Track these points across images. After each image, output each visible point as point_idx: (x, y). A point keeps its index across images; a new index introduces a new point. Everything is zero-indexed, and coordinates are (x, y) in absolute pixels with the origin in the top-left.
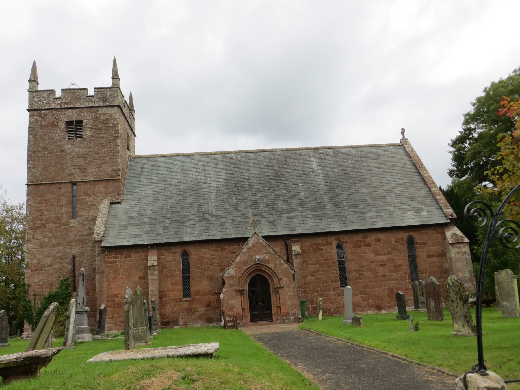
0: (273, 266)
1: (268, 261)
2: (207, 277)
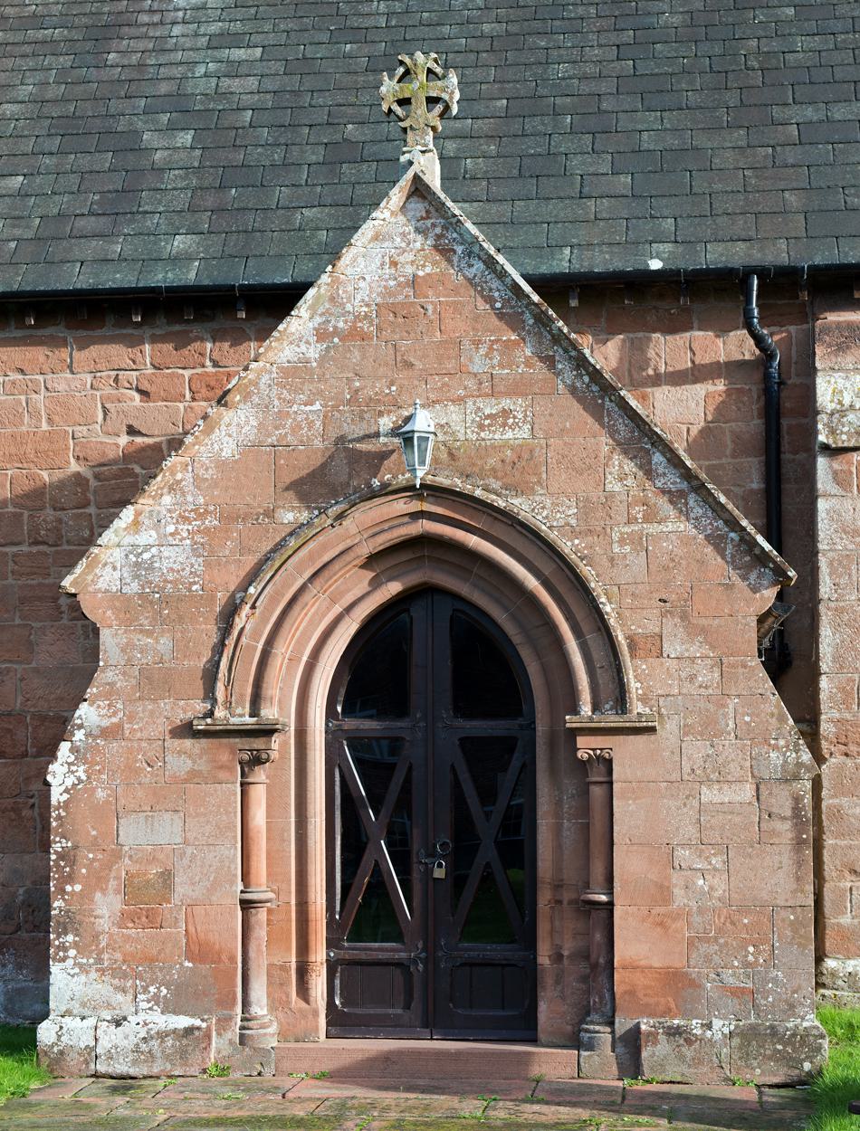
0: (569, 513)
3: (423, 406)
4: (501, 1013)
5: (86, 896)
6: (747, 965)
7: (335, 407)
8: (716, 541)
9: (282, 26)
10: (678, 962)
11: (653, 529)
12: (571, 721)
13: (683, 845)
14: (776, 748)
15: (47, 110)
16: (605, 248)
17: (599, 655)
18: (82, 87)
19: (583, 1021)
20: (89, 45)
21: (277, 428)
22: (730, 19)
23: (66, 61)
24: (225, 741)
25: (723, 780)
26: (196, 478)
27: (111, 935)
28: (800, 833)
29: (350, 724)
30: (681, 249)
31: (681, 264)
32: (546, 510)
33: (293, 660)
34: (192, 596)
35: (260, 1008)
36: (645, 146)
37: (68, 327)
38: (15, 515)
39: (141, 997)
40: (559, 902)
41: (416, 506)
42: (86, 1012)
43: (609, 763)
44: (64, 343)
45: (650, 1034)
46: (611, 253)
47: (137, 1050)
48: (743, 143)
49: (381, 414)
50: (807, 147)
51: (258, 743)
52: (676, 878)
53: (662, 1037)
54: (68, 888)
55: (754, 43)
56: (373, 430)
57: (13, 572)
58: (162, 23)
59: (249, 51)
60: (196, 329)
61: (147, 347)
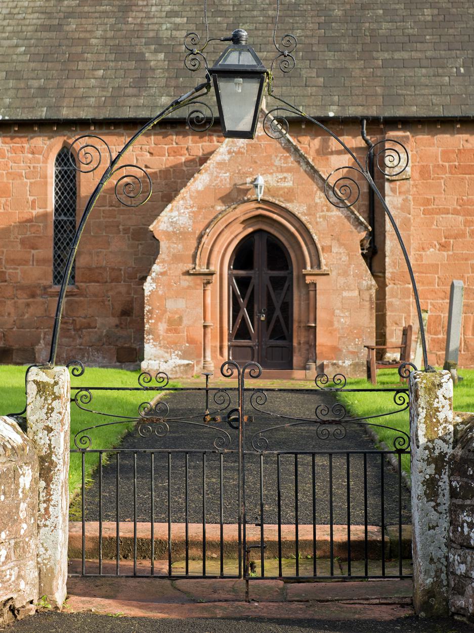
0: (304, 208)
1: (290, 194)
2: (126, 230)
3: (261, 175)
4: (281, 362)
5: (156, 324)
6: (355, 344)
7: (233, 175)
8: (348, 218)
9: (194, 9)
10: (335, 344)
11: (329, 214)
12: (304, 272)
13: (337, 309)
14: (365, 280)
15: (109, 42)
16: (314, 107)
17: (313, 251)
18: (120, 33)
19: (307, 362)
20: (121, 14)
21: (215, 180)
22: (359, 14)
23: (112, 21)
24: (199, 277)
25: (349, 290)
26: (190, 195)
27: (163, 336)
28: (371, 305)
29: (235, 272)
30: (340, 108)
31: (340, 114)
32: (297, 208)
33: (219, 252)
34: (189, 233)
35: (209, 359)
36: (328, 66)
37: (124, 129)
38: (104, 196)
39: (173, 354)
40: (300, 327)
41: (258, 205)
42: (156, 359)
43: (315, 284)
44: (123, 135)
45: (326, 365)
46: (317, 109)
47: (172, 370)
48: (362, 67)
49: (247, 177)
50: (385, 69)
51: (209, 277)
52: (335, 319)
53: (330, 366)
54: (150, 321)
55: (367, 25)
56: (245, 182)
57: (103, 216)
58: (147, 5)
59: (182, 19)
60: (170, 131)
61: (152, 137)
